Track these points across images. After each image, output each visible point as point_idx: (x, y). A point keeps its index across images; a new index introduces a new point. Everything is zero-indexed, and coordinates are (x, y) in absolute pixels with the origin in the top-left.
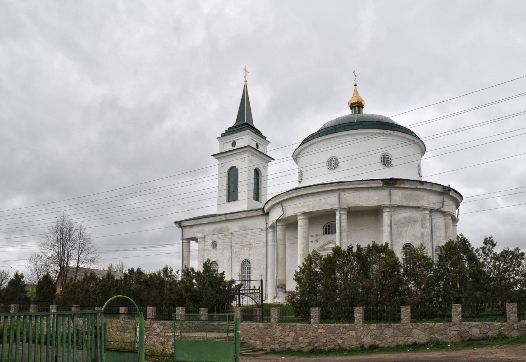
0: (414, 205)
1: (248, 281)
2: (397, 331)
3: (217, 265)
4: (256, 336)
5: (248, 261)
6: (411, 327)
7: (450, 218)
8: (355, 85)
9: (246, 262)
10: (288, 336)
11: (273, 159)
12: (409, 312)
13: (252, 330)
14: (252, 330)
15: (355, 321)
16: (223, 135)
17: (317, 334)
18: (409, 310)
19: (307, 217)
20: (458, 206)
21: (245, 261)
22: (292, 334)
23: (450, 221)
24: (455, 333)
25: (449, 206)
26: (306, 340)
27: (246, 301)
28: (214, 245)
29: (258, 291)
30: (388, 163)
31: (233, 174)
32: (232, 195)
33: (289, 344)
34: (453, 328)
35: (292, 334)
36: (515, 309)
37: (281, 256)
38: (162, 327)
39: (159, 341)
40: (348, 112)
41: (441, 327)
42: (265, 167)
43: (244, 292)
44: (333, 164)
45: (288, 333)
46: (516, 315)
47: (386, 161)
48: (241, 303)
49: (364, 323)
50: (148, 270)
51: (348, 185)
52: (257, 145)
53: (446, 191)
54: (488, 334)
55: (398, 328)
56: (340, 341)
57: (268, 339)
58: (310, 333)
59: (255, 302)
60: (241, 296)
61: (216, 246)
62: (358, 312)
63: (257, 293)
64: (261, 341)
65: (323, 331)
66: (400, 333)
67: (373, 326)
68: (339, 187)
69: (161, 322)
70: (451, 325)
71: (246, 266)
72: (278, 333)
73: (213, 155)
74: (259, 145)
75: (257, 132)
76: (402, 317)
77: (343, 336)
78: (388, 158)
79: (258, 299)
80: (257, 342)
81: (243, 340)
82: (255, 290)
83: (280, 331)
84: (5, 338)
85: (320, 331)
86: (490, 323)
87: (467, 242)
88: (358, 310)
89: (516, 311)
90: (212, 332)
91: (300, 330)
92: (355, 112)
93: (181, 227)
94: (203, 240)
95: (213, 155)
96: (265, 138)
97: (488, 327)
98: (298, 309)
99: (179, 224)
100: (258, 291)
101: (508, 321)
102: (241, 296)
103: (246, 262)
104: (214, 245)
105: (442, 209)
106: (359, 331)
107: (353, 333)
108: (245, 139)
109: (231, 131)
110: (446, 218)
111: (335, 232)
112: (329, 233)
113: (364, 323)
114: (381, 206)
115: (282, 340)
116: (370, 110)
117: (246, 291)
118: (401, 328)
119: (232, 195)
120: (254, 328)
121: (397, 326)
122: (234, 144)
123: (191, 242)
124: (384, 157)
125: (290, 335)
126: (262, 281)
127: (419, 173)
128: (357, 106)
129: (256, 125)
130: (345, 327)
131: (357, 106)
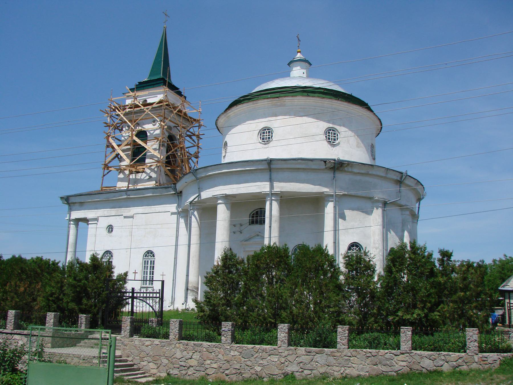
0: (364, 195)
2: (331, 359)
4: (150, 356)
6: (349, 354)
7: (408, 213)
9: (150, 253)
10: (191, 358)
12: (347, 335)
13: (144, 348)
14: (144, 348)
15: (279, 342)
17: (228, 358)
18: (347, 332)
20: (419, 200)
22: (196, 356)
23: (409, 218)
24: (404, 364)
25: (407, 197)
26: (215, 365)
27: (141, 307)
28: (110, 229)
29: (158, 295)
30: (335, 140)
33: (192, 368)
34: (401, 357)
35: (196, 356)
36: (476, 337)
37: (145, 85)
41: (386, 356)
43: (138, 295)
44: (266, 135)
45: (191, 354)
47: (331, 136)
49: (289, 345)
50: (28, 257)
53: (401, 179)
54: (443, 368)
55: (332, 355)
56: (258, 369)
57: (165, 361)
58: (220, 356)
59: (153, 309)
60: (135, 300)
61: (112, 231)
62: (282, 331)
63: (156, 297)
65: (236, 353)
66: (335, 361)
67: (301, 350)
68: (270, 168)
70: (398, 354)
71: (150, 259)
75: (173, 88)
76: (339, 340)
77: (262, 362)
79: (157, 306)
81: (132, 361)
82: (153, 293)
83: (182, 351)
85: (232, 353)
86: (446, 353)
88: (282, 328)
90: (92, 347)
93: (68, 203)
94: (96, 222)
97: (443, 358)
98: (206, 322)
99: (67, 200)
100: (158, 295)
101: (468, 351)
102: (135, 300)
103: (150, 253)
104: (110, 229)
105: (399, 202)
106: (282, 355)
107: (275, 358)
110: (404, 213)
111: (264, 222)
112: (257, 222)
113: (289, 345)
115: (182, 363)
117: (142, 295)
118: (336, 354)
121: (332, 352)
123: (80, 223)
125: (193, 357)
126: (163, 282)
129: (175, 82)
130: (264, 351)
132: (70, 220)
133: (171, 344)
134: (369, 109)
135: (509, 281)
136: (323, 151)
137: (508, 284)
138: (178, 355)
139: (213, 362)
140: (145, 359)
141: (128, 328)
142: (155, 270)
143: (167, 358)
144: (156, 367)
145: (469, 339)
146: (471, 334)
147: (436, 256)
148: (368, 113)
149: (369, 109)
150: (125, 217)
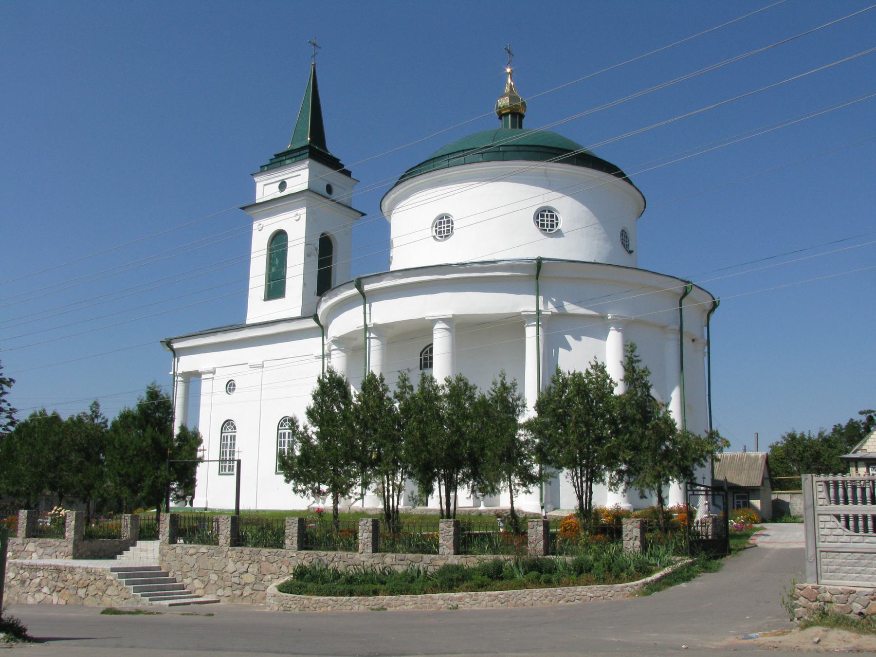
1: (226, 461)
3: (235, 428)
5: (232, 424)
10: (247, 572)
11: (363, 214)
12: (452, 533)
15: (360, 546)
18: (452, 528)
22: (254, 569)
30: (552, 226)
33: (247, 587)
35: (254, 569)
38: (41, 550)
39: (19, 577)
45: (246, 565)
46: (638, 543)
47: (546, 220)
51: (401, 277)
52: (329, 189)
57: (214, 577)
61: (234, 389)
64: (203, 582)
72: (231, 567)
74: (334, 188)
75: (333, 163)
80: (196, 581)
84: (870, 523)
88: (365, 525)
89: (639, 535)
91: (267, 560)
94: (210, 376)
96: (348, 173)
104: (230, 386)
114: (519, 315)
115: (236, 580)
120: (191, 555)
122: (283, 185)
132: (175, 375)
133: (222, 552)
134: (621, 175)
135: (865, 442)
136: (531, 245)
137: (864, 447)
138: (231, 567)
139: (275, 576)
140: (189, 574)
141: (168, 529)
142: (236, 442)
143: (216, 572)
144: (203, 586)
145: (627, 535)
146: (630, 527)
147: (517, 394)
148: (317, 69)
149: (621, 175)
150: (252, 367)
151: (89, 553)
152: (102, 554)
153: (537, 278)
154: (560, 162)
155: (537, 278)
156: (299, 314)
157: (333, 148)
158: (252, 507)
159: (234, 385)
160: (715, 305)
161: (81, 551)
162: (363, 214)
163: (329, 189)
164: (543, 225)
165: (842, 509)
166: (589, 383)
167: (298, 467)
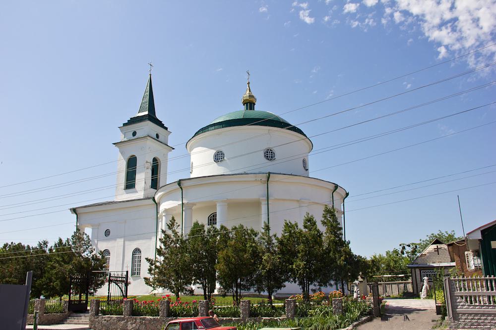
3: (140, 252)
5: (108, 252)
8: (249, 83)
11: (173, 149)
16: (125, 125)
19: (226, 204)
21: (136, 250)
30: (272, 157)
31: (132, 163)
32: (130, 184)
40: (243, 108)
42: (165, 156)
48: (68, 296)
52: (157, 136)
61: (109, 234)
69: (425, 266)
73: (114, 144)
75: (159, 123)
78: (272, 153)
82: (118, 277)
87: (340, 225)
92: (247, 109)
95: (114, 144)
96: (166, 129)
99: (74, 210)
108: (148, 127)
109: (134, 121)
116: (261, 108)
119: (130, 184)
122: (134, 134)
124: (267, 152)
127: (304, 167)
128: (250, 104)
131: (250, 104)
142: (141, 268)
151: (46, 322)
152: (53, 322)
153: (268, 182)
154: (288, 129)
155: (268, 182)
156: (142, 198)
157: (159, 116)
158: (130, 295)
159: (109, 232)
160: (347, 194)
161: (42, 321)
162: (173, 149)
163: (157, 136)
164: (267, 157)
165: (423, 294)
166: (293, 233)
167: (161, 277)
